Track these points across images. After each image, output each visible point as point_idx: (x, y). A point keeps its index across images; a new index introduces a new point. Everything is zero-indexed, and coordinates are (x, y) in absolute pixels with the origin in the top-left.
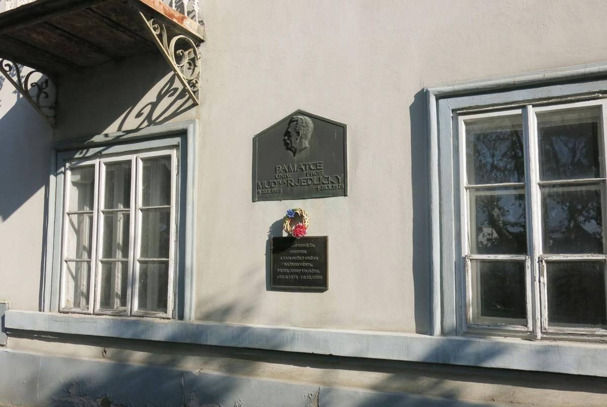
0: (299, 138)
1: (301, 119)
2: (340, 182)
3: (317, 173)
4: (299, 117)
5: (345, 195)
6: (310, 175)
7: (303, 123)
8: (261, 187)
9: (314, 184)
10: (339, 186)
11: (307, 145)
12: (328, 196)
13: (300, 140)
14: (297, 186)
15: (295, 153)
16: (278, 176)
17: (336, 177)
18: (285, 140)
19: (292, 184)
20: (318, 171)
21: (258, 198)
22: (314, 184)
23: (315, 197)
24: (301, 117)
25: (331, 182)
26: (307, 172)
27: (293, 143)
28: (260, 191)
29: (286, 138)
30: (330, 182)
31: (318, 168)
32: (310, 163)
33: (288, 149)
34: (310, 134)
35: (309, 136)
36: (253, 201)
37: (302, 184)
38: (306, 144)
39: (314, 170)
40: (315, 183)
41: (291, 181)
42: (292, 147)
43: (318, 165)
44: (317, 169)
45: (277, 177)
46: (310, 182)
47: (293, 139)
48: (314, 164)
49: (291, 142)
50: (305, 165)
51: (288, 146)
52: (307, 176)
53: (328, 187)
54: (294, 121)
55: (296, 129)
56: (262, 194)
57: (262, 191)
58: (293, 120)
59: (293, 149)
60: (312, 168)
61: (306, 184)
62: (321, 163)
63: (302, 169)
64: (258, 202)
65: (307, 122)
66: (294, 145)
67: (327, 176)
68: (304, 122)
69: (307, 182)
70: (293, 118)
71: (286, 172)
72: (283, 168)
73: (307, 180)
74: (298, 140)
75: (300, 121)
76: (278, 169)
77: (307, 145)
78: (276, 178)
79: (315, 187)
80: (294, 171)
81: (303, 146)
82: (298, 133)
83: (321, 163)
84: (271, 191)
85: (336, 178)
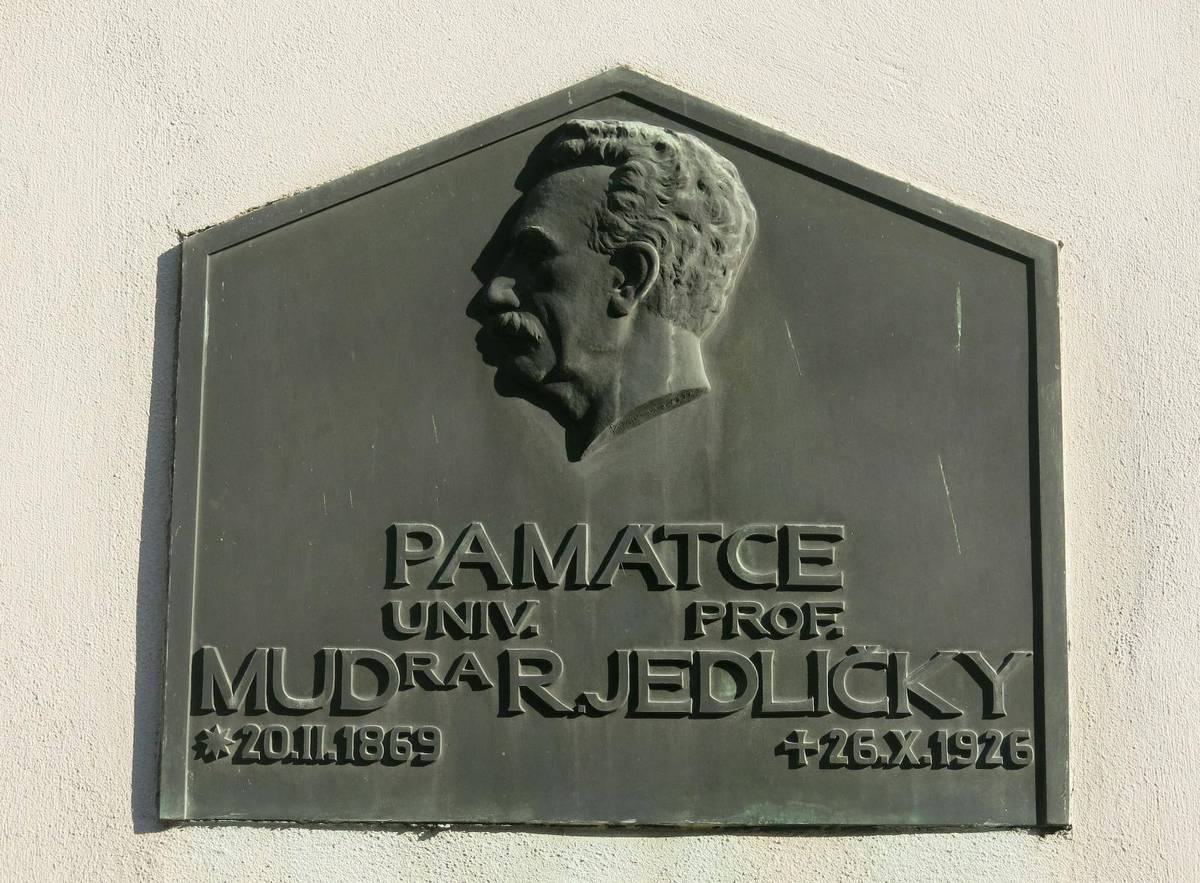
0: (632, 309)
1: (660, 147)
2: (1000, 705)
3: (789, 615)
4: (633, 126)
5: (1046, 823)
6: (728, 634)
7: (674, 181)
8: (234, 701)
9: (757, 711)
10: (988, 742)
11: (703, 378)
12: (894, 819)
13: (639, 324)
14: (593, 713)
15: (580, 435)
16: (415, 615)
17: (964, 661)
18: (482, 308)
19: (554, 695)
20: (795, 602)
21: (197, 798)
22: (757, 711)
23: (763, 820)
24: (656, 131)
25: (915, 699)
26: (701, 600)
27: (573, 333)
28: (224, 734)
29: (502, 290)
30: (906, 706)
31: (802, 573)
32: (723, 530)
33: (512, 383)
34: (731, 281)
35: (722, 301)
36: (150, 815)
37: (652, 700)
38: (690, 356)
39: (768, 586)
40: (774, 701)
41: (545, 665)
42: (560, 373)
43: (802, 547)
44: (785, 587)
45: (402, 623)
46: (722, 691)
47: (577, 309)
48: (764, 538)
49: (556, 331)
50: (682, 541)
51: (514, 362)
52: (691, 633)
53: (893, 742)
54: (591, 156)
55: (609, 228)
56: (238, 759)
57: (242, 736)
58: (576, 144)
59: (567, 391)
60: (746, 571)
61: (682, 701)
62: (834, 538)
63: (649, 574)
64: (197, 835)
65: (715, 182)
66: (580, 362)
67: (878, 652)
68: (689, 174)
69: (696, 691)
70: (579, 132)
71: (493, 582)
72: (465, 549)
73: (695, 667)
74: (625, 324)
75: (646, 163)
76: (410, 548)
77: (703, 378)
78: (391, 631)
79: (773, 732)
80: (572, 584)
81: (670, 384)
82: (631, 264)
83: (834, 538)
84: (340, 739)
85: (962, 676)
